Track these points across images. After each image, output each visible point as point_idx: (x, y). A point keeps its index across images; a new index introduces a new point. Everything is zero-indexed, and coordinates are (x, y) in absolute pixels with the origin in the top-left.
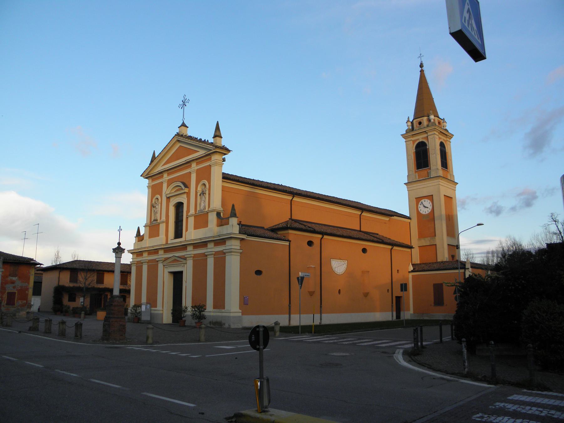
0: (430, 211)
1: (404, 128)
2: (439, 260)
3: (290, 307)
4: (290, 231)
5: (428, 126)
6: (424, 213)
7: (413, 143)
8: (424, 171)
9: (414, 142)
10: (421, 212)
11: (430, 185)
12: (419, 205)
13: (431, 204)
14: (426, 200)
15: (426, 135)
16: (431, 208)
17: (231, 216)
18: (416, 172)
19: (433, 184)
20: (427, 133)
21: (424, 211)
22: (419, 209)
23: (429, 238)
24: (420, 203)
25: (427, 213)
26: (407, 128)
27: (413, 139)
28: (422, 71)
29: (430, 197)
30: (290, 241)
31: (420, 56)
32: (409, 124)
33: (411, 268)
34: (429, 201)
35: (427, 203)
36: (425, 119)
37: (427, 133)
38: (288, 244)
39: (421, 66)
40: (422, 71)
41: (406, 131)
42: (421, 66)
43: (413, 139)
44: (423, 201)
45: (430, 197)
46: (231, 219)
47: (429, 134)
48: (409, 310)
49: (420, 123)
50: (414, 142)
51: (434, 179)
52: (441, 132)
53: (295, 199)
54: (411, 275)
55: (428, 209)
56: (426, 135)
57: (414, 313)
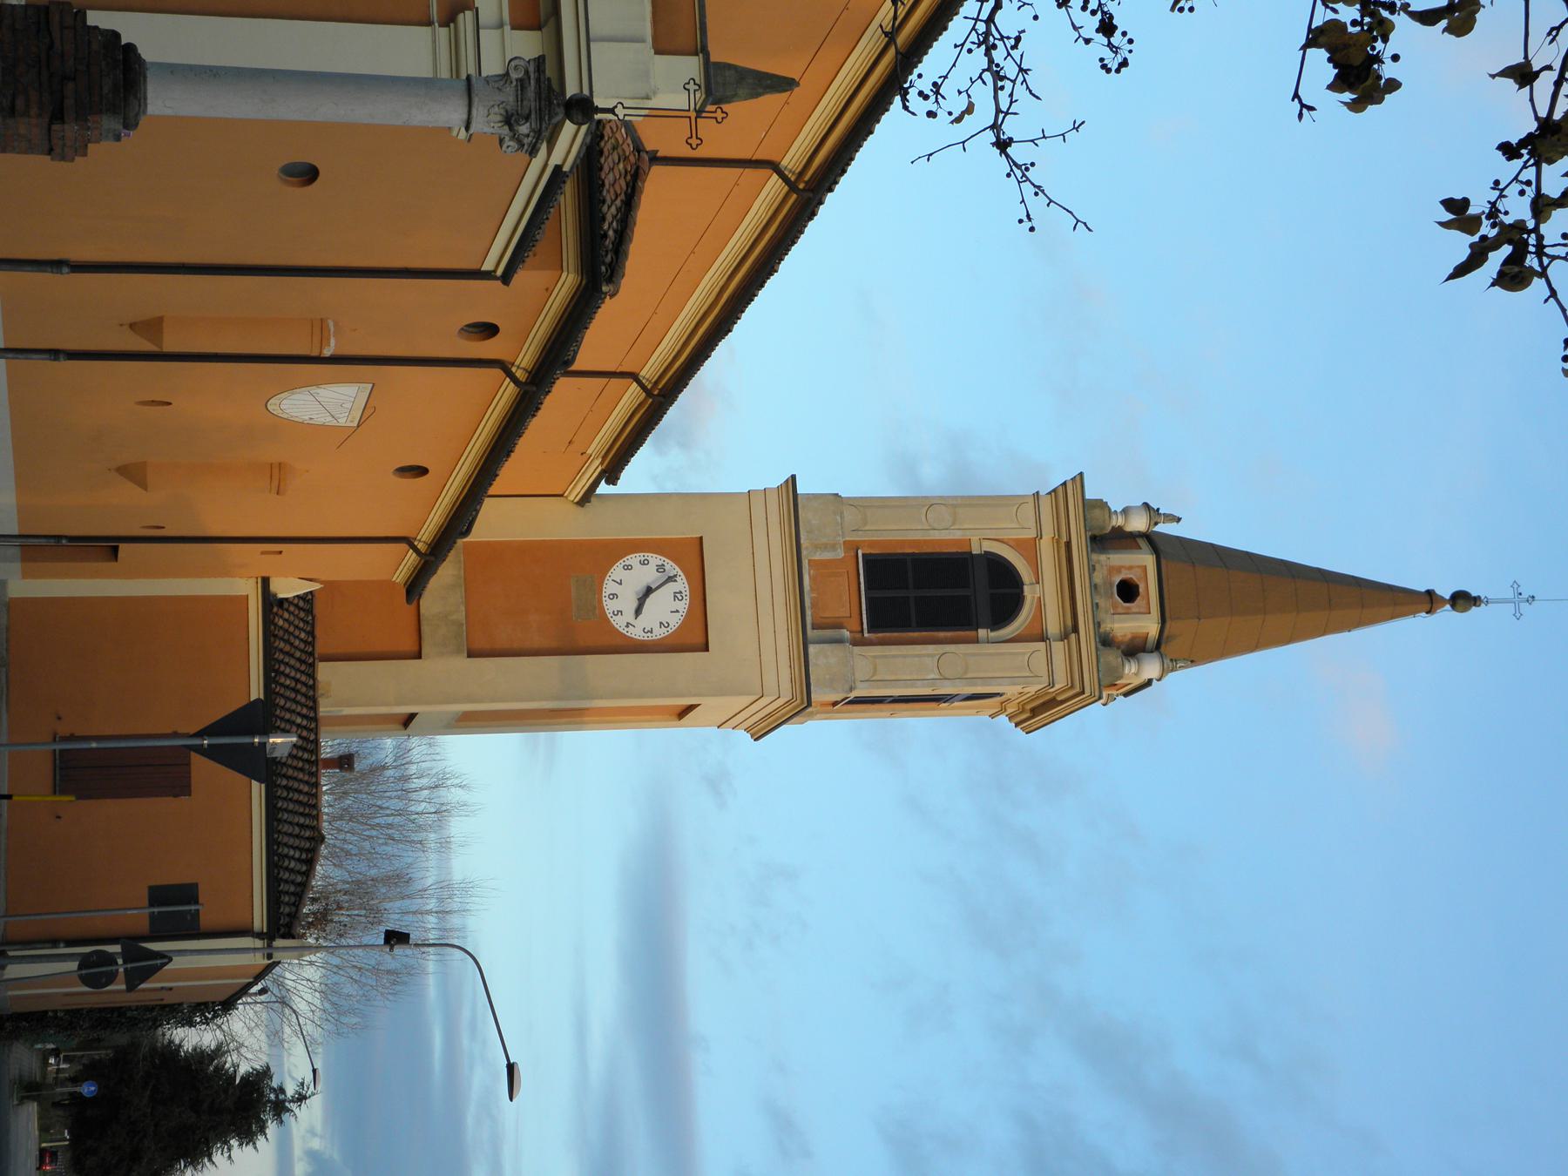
0: (619, 623)
1: (1118, 491)
2: (324, 671)
3: (56, 265)
4: (568, 282)
5: (1106, 641)
6: (609, 587)
7: (1018, 545)
8: (846, 598)
9: (1029, 548)
10: (617, 571)
11: (767, 639)
12: (655, 559)
13: (659, 633)
14: (683, 606)
15: (1053, 626)
16: (636, 633)
17: (713, 72)
18: (853, 547)
19: (768, 656)
20: (1064, 637)
21: (621, 586)
22: (633, 559)
23: (461, 616)
24: (672, 568)
25: (610, 606)
26: (1116, 506)
27: (1046, 550)
28: (1429, 601)
29: (694, 637)
30: (506, 278)
31: (1522, 599)
32: (1138, 524)
33: (287, 588)
34: (675, 621)
35: (666, 613)
36: (1150, 626)
37: (1064, 637)
38: (488, 266)
39: (1462, 600)
40: (1429, 601)
41: (1101, 505)
42: (1462, 600)
43: (1046, 550)
44: (681, 584)
45: (694, 637)
46: (690, 67)
47: (1058, 647)
48: (25, 575)
49: (1128, 591)
50: (1029, 548)
51: (798, 671)
52: (1068, 545)
53: (774, 186)
54: (247, 588)
55: (629, 615)
56: (1053, 626)
57: (14, 606)
